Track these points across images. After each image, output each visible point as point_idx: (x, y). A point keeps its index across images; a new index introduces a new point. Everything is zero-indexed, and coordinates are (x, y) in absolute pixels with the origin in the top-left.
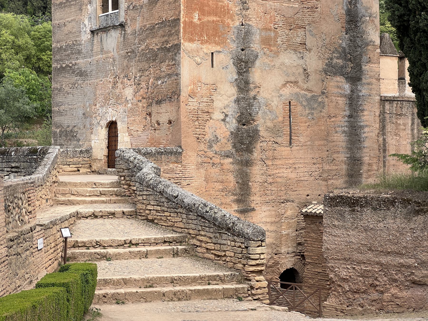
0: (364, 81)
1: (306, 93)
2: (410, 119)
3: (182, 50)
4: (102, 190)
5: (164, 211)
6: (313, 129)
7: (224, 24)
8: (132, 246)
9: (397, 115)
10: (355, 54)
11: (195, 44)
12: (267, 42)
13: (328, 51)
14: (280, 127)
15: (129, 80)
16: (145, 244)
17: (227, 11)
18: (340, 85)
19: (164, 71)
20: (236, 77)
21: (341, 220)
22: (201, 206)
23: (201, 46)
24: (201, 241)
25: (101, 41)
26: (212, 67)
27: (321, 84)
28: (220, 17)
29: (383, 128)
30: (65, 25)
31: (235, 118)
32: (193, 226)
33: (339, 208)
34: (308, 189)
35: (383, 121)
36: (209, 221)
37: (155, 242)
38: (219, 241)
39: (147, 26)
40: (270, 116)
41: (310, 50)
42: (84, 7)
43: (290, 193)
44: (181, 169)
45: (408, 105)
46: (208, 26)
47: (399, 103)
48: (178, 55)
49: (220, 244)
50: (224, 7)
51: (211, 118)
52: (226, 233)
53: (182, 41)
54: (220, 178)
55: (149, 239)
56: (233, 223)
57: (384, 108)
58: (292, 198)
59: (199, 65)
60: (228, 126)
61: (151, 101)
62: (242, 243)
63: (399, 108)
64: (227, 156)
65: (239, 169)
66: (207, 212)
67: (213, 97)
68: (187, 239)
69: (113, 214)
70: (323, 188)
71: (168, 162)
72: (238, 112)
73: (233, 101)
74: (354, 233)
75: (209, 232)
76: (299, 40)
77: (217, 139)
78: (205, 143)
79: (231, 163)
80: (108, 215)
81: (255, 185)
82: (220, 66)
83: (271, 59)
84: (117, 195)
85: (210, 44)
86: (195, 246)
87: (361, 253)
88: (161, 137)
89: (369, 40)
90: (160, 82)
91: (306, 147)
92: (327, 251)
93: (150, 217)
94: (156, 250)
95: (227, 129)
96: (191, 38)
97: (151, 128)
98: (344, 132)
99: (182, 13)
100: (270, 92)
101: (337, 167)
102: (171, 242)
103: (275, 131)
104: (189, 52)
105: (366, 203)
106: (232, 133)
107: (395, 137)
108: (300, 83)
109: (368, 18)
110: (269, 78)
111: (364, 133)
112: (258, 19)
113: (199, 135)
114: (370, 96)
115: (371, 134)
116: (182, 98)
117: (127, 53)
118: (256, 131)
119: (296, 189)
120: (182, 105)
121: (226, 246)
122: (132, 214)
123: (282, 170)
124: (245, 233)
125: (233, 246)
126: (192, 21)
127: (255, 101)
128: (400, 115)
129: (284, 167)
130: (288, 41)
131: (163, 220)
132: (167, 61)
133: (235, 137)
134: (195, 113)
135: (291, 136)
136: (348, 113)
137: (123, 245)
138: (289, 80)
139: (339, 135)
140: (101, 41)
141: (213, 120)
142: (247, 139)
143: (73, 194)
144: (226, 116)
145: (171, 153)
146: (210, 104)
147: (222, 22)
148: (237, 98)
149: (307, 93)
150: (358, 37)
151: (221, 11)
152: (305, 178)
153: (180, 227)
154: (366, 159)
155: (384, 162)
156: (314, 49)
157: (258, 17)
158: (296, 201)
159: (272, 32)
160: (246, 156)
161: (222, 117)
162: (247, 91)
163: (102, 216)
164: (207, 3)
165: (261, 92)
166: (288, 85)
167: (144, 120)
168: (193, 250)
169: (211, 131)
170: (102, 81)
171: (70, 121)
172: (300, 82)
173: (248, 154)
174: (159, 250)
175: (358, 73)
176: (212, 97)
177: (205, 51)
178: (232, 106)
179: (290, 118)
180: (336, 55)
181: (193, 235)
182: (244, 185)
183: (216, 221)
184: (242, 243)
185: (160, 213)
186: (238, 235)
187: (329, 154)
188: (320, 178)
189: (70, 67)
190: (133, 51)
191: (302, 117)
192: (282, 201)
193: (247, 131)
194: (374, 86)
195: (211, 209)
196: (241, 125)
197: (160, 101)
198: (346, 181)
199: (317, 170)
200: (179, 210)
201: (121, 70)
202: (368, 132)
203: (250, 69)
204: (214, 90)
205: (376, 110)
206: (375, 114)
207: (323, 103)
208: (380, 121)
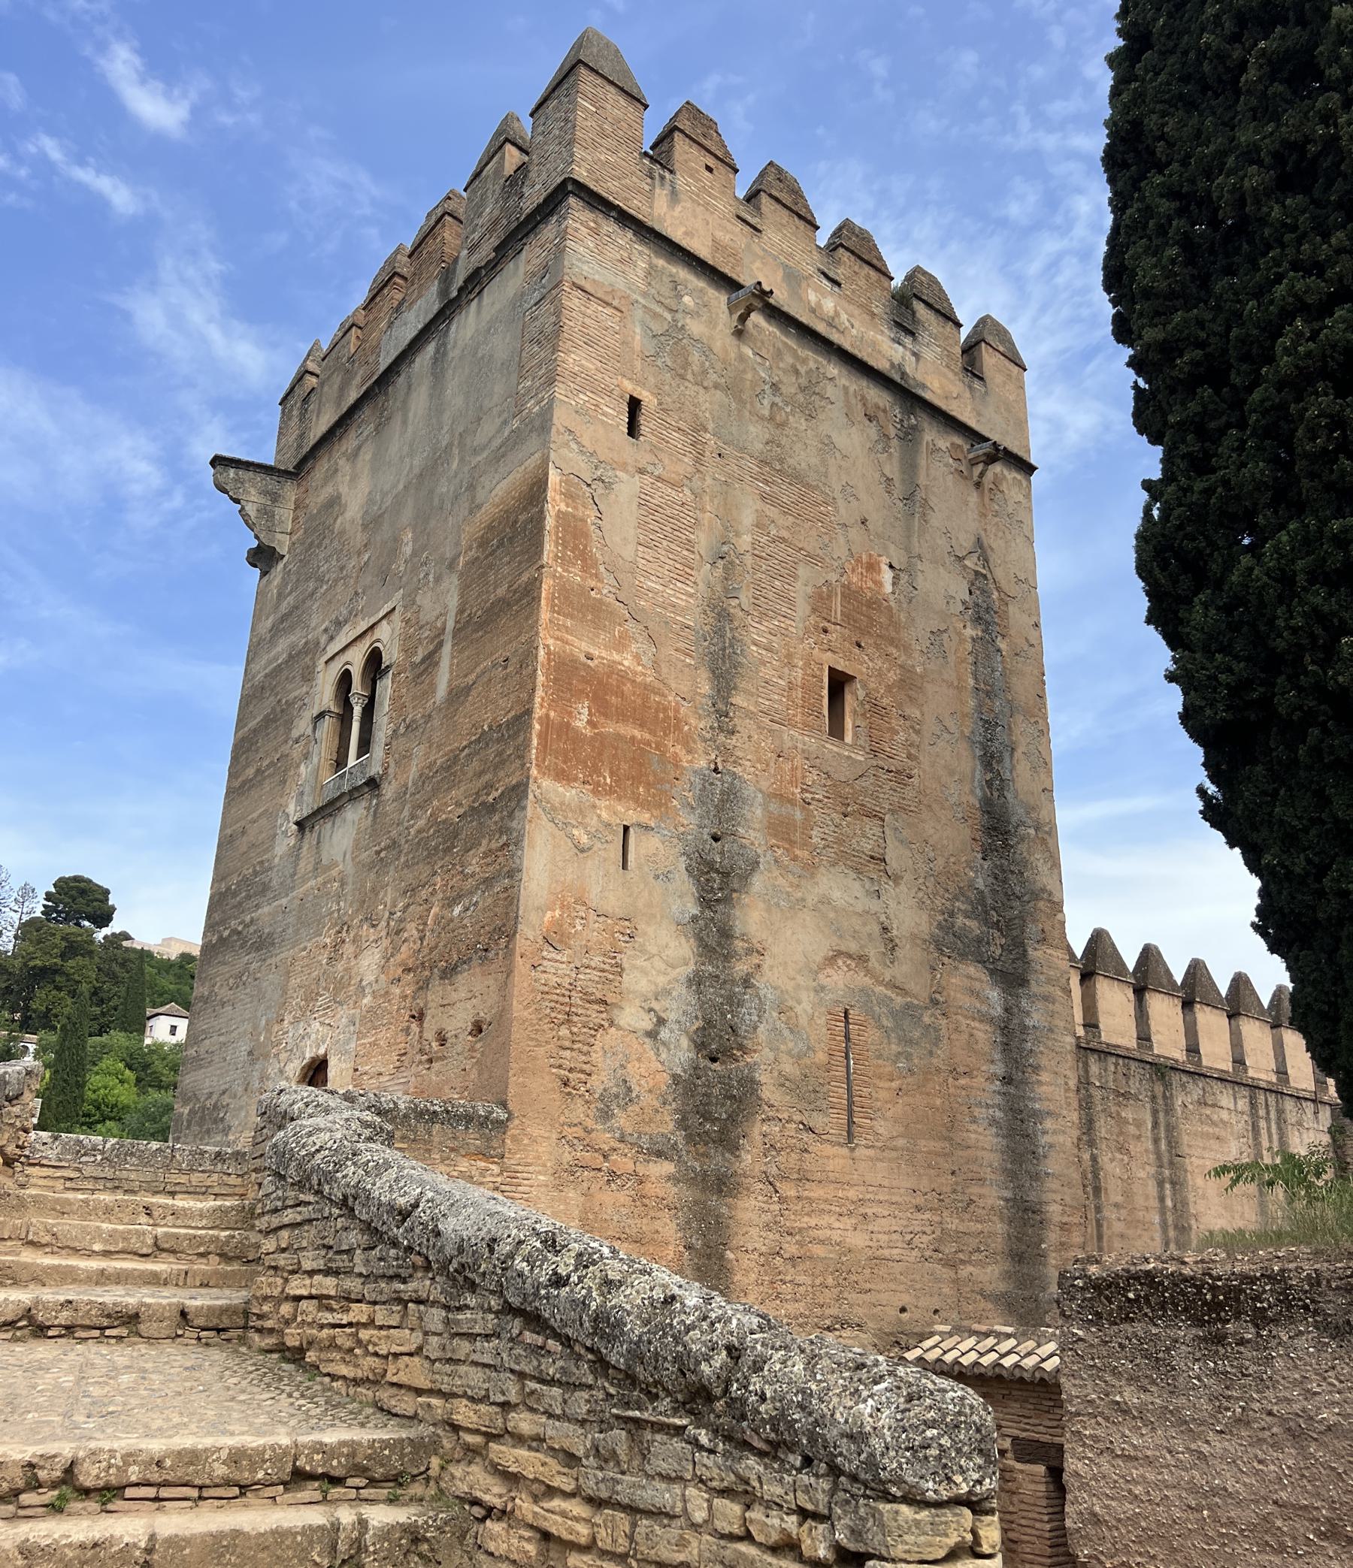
0: (1034, 988)
1: (889, 993)
2: (1149, 1111)
3: (531, 796)
4: (166, 1234)
5: (348, 1299)
6: (911, 1100)
7: (663, 754)
8: (77, 1506)
9: (1119, 1094)
10: (1008, 914)
11: (574, 791)
12: (781, 830)
13: (941, 892)
14: (821, 1081)
15: (374, 926)
16: (165, 1493)
17: (673, 721)
18: (972, 988)
19: (473, 875)
20: (695, 911)
21: (1153, 1382)
22: (525, 1249)
23: (592, 799)
24: (512, 1479)
25: (318, 843)
26: (624, 866)
27: (929, 976)
28: (652, 732)
29: (1088, 1125)
30: (243, 833)
31: (687, 1033)
32: (475, 1378)
33: (1139, 1328)
34: (902, 1287)
35: (1086, 1105)
36: (567, 1342)
37: (236, 1476)
38: (629, 1487)
39: (439, 762)
40: (791, 1045)
41: (896, 879)
42: (292, 773)
43: (853, 1297)
44: (499, 1179)
45: (1142, 1071)
46: (616, 749)
47: (1121, 1061)
48: (517, 813)
49: (632, 1510)
50: (665, 709)
51: (612, 1024)
52: (680, 1430)
53: (534, 772)
54: (634, 1226)
55: (192, 1457)
56: (730, 1348)
57: (1087, 1072)
58: (858, 1313)
59: (582, 851)
60: (664, 1056)
61: (427, 973)
62: (804, 1514)
63: (1120, 1077)
64: (659, 1154)
65: (696, 1203)
66: (559, 1281)
67: (624, 959)
68: (435, 1462)
69: (130, 1320)
70: (946, 1290)
71: (452, 1150)
72: (696, 1017)
73: (683, 979)
74: (1231, 1446)
75: (563, 1417)
76: (867, 846)
77: (626, 1094)
78: (587, 1102)
79: (669, 1179)
80: (105, 1322)
81: (746, 1261)
82: (646, 869)
83: (796, 881)
84: (224, 1257)
85: (619, 798)
86: (478, 1512)
87: (1282, 1549)
88: (447, 1082)
89: (1039, 885)
90: (457, 910)
91: (894, 1154)
92: (1091, 1530)
93: (293, 1337)
94: (217, 1537)
95: (662, 1063)
96: (564, 771)
97: (418, 1057)
98: (993, 1122)
99: (540, 693)
100: (792, 973)
101: (979, 1226)
102: (336, 1481)
103: (805, 1090)
104: (554, 809)
105: (1285, 1300)
106: (675, 1078)
107: (1118, 1156)
108: (874, 963)
109: (1032, 831)
110: (789, 932)
111: (1045, 1133)
112: (758, 766)
113: (570, 1070)
114: (1051, 1030)
115: (1061, 1139)
116: (521, 944)
117: (378, 853)
118: (750, 1085)
119: (868, 1286)
120: (521, 966)
121: (674, 1532)
122: (226, 1322)
123: (826, 1217)
124: (832, 1434)
125: (732, 1537)
126: (568, 724)
127: (749, 990)
128: (1126, 1095)
129: (833, 1208)
130: (840, 842)
131: (338, 1348)
132: (484, 842)
133: (685, 1094)
134: (561, 999)
135: (851, 1114)
136: (999, 1069)
137: (16, 1493)
138: (843, 948)
139: (981, 1130)
140: (318, 843)
141: (619, 1028)
142: (723, 1105)
143: (31, 1243)
144: (661, 1021)
145: (468, 1119)
146: (611, 977)
147: (657, 748)
148: (696, 973)
149: (893, 996)
150: (1012, 872)
151: (657, 717)
152: (895, 1251)
153: (409, 1388)
154: (1054, 1211)
155: (1099, 1225)
156: (908, 877)
157: (759, 761)
158: (870, 1325)
159: (797, 809)
160: (717, 1160)
161: (647, 1023)
162: (727, 958)
163: (69, 1329)
164: (618, 687)
165: (765, 967)
166: (840, 962)
167: (401, 1037)
168: (463, 1536)
169: (612, 1063)
170: (305, 949)
171: (215, 1079)
172: (873, 960)
173: (723, 1155)
174: (237, 1533)
175: (1019, 963)
176: (619, 956)
177: (604, 815)
178: (680, 995)
179: (847, 1057)
180: (963, 907)
181: (470, 1439)
182: (709, 1257)
183: (610, 1339)
184: (804, 1514)
185: (331, 1310)
186: (775, 1445)
187: (957, 1183)
188: (936, 1255)
189: (240, 933)
190: (394, 842)
191: (880, 1062)
192: (828, 1322)
193: (724, 1080)
194: (1058, 1007)
195: (584, 1261)
196: (704, 1057)
197: (454, 969)
198: (1007, 1272)
199: (928, 1230)
200: (412, 1286)
201: (355, 906)
202: (1055, 1132)
203: (734, 895)
204: (627, 938)
205: (1068, 1073)
206: (1066, 1084)
207: (937, 1030)
208: (1080, 1106)
